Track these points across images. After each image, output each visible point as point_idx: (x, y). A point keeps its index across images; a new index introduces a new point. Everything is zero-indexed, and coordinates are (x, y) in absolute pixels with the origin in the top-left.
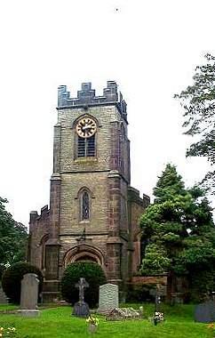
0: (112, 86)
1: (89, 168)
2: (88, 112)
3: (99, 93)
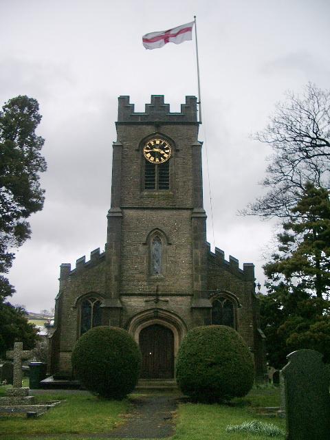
0: (191, 103)
2: (161, 131)
3: (175, 109)
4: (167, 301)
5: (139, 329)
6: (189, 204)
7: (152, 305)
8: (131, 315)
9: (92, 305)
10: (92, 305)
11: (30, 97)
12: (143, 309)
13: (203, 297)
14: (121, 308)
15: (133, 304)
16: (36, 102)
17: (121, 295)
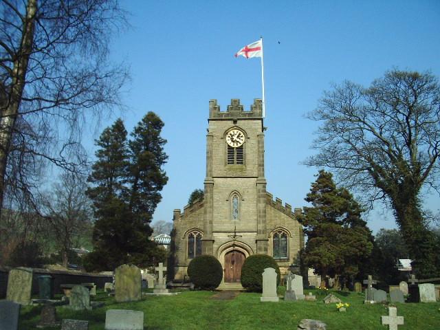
1: (239, 174)
6: (255, 174)
9: (195, 236)
10: (195, 236)
11: (147, 114)
12: (227, 241)
15: (221, 238)
16: (152, 112)
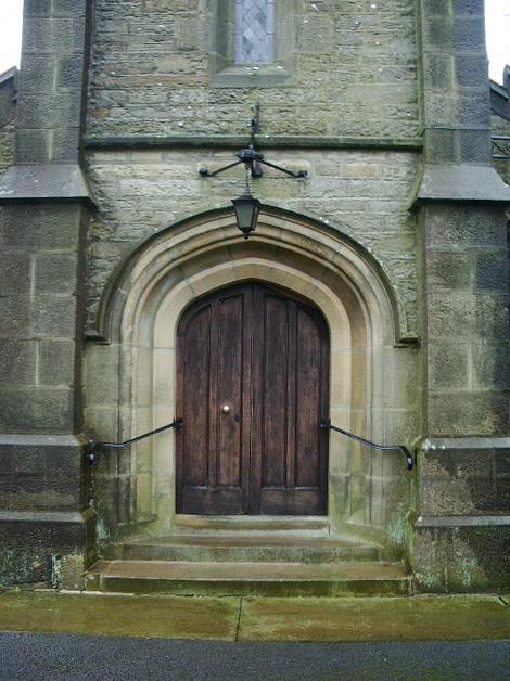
4: (302, 174)
5: (175, 301)
7: (236, 181)
8: (138, 234)
13: (469, 156)
14: (87, 206)
15: (146, 188)
17: (88, 149)
